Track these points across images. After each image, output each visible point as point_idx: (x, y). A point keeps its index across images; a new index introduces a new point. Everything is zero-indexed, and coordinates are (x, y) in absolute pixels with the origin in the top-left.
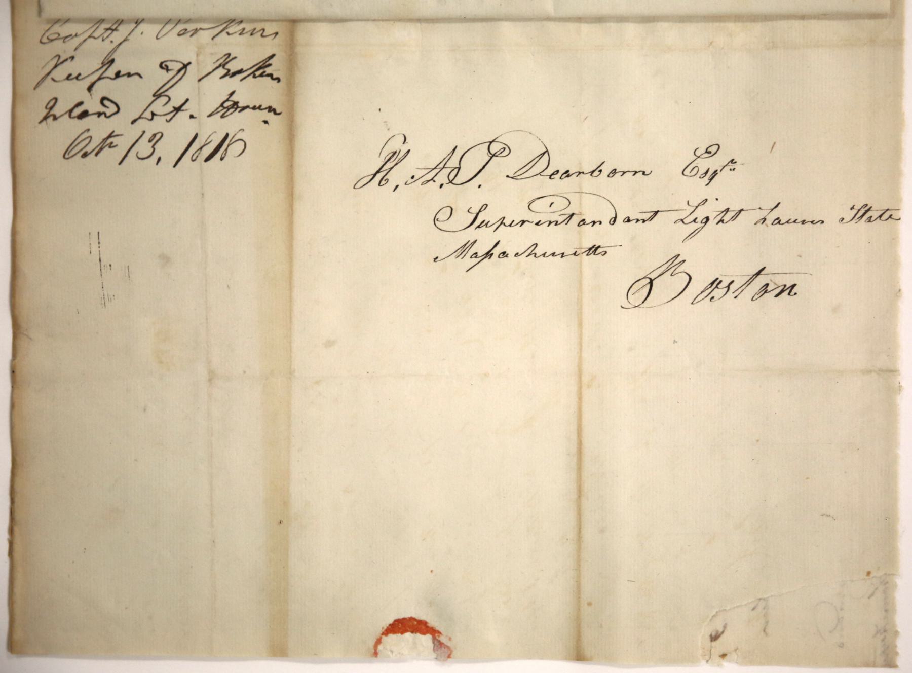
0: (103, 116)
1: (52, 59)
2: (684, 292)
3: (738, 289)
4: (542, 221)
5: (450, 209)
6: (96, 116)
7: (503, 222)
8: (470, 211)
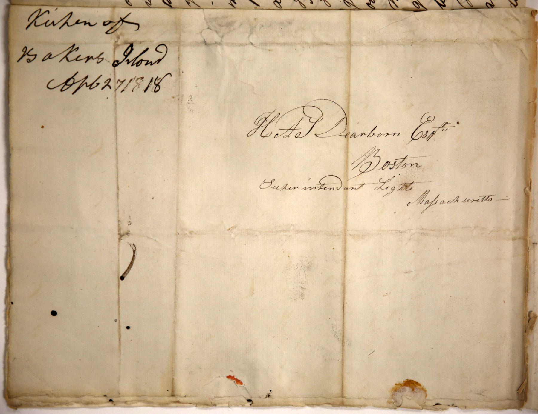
0: (88, 25)
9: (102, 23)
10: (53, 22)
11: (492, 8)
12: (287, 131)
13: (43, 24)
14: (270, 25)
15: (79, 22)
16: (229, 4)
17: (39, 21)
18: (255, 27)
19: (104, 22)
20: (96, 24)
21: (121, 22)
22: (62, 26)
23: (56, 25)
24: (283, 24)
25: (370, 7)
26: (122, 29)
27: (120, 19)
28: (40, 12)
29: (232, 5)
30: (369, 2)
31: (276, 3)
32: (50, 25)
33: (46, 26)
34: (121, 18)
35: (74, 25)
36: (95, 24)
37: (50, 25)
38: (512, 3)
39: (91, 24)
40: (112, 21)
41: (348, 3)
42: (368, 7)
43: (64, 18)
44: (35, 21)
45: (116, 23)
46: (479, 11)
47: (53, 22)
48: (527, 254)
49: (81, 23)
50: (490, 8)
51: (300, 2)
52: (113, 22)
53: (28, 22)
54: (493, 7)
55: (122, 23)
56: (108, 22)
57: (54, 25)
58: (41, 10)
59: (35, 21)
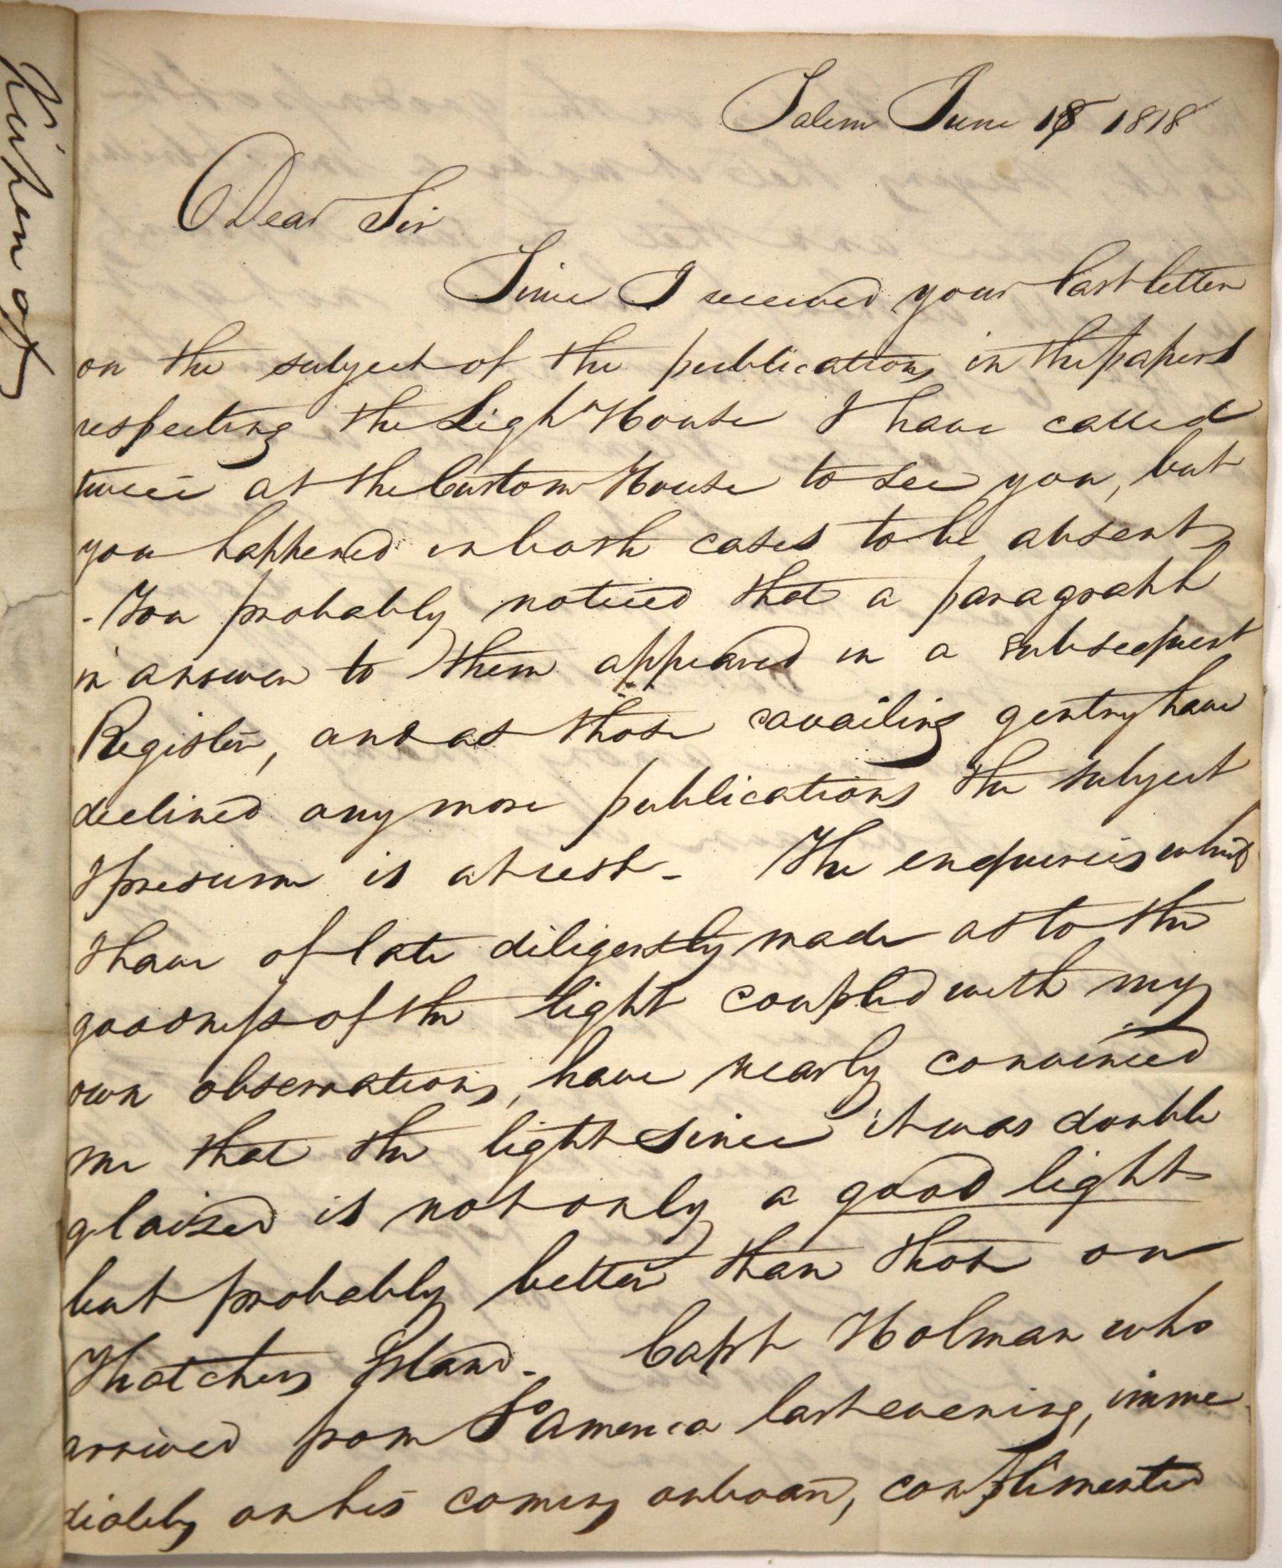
0: (15, 243)
1: (542, 845)
2: (846, 1119)
3: (36, 175)
4: (84, 1462)
5: (146, 702)
6: (95, 471)
7: (122, 956)
8: (523, 249)
9: (21, 288)
10: (21, 139)
11: (65, 1456)
12: (811, 1240)
13: (15, 109)
14: (18, 794)
15: (23, 218)
16: (86, 670)
17: (24, 98)
18: (13, 748)
19: (23, 293)
20: (19, 268)
21: (25, 344)
22: (10, 166)
23: (13, 145)
24: (22, 832)
25: (74, 1091)
26: (5, 345)
27: (32, 341)
28: (52, 100)
29: (82, 678)
30: (86, 1088)
31: (86, 810)
32: (12, 127)
33: (8, 116)
34: (37, 343)
35: (14, 200)
36: (18, 264)
37: (12, 127)
38: (76, 1512)
39: (18, 254)
40: (28, 317)
41: (86, 1026)
42: (73, 1086)
43: (33, 171)
44: (24, 83)
45: (21, 329)
46: (55, 1414)
47: (21, 139)
48: (30, 1357)
49: (21, 223)
50: (1259, 784)
51: (88, 883)
52: (24, 319)
53: (19, 62)
54: (67, 1458)
55: (21, 347)
56: (24, 305)
57: (11, 140)
58: (59, 101)
59: (24, 83)
